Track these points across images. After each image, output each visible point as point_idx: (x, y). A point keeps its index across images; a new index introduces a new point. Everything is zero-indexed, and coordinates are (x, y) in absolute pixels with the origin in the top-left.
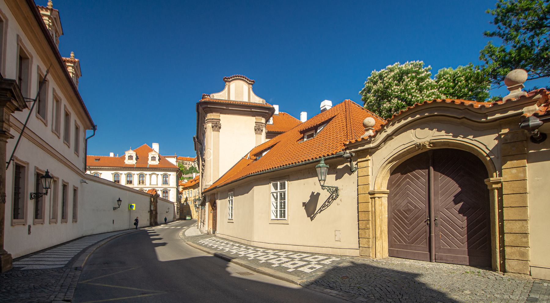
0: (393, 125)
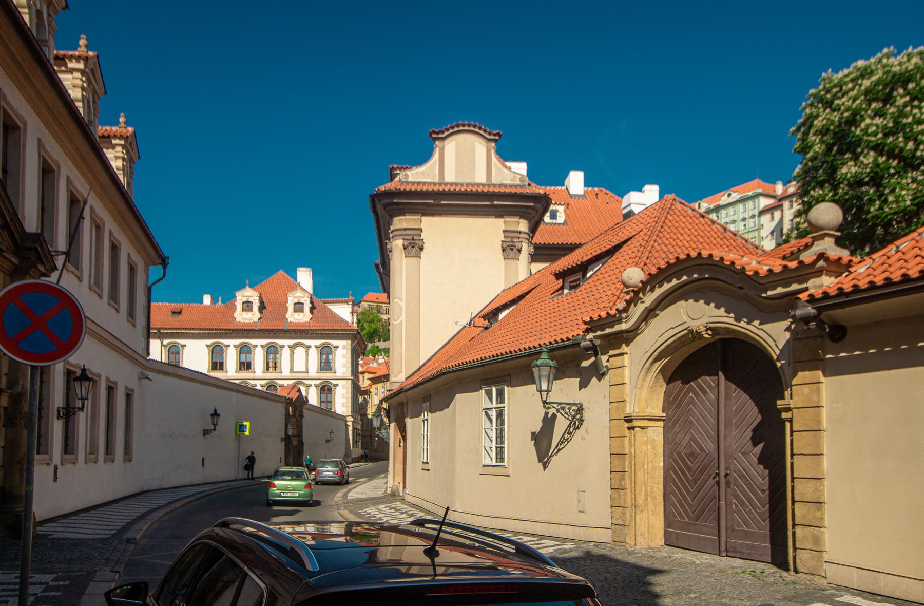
0: (652, 290)
